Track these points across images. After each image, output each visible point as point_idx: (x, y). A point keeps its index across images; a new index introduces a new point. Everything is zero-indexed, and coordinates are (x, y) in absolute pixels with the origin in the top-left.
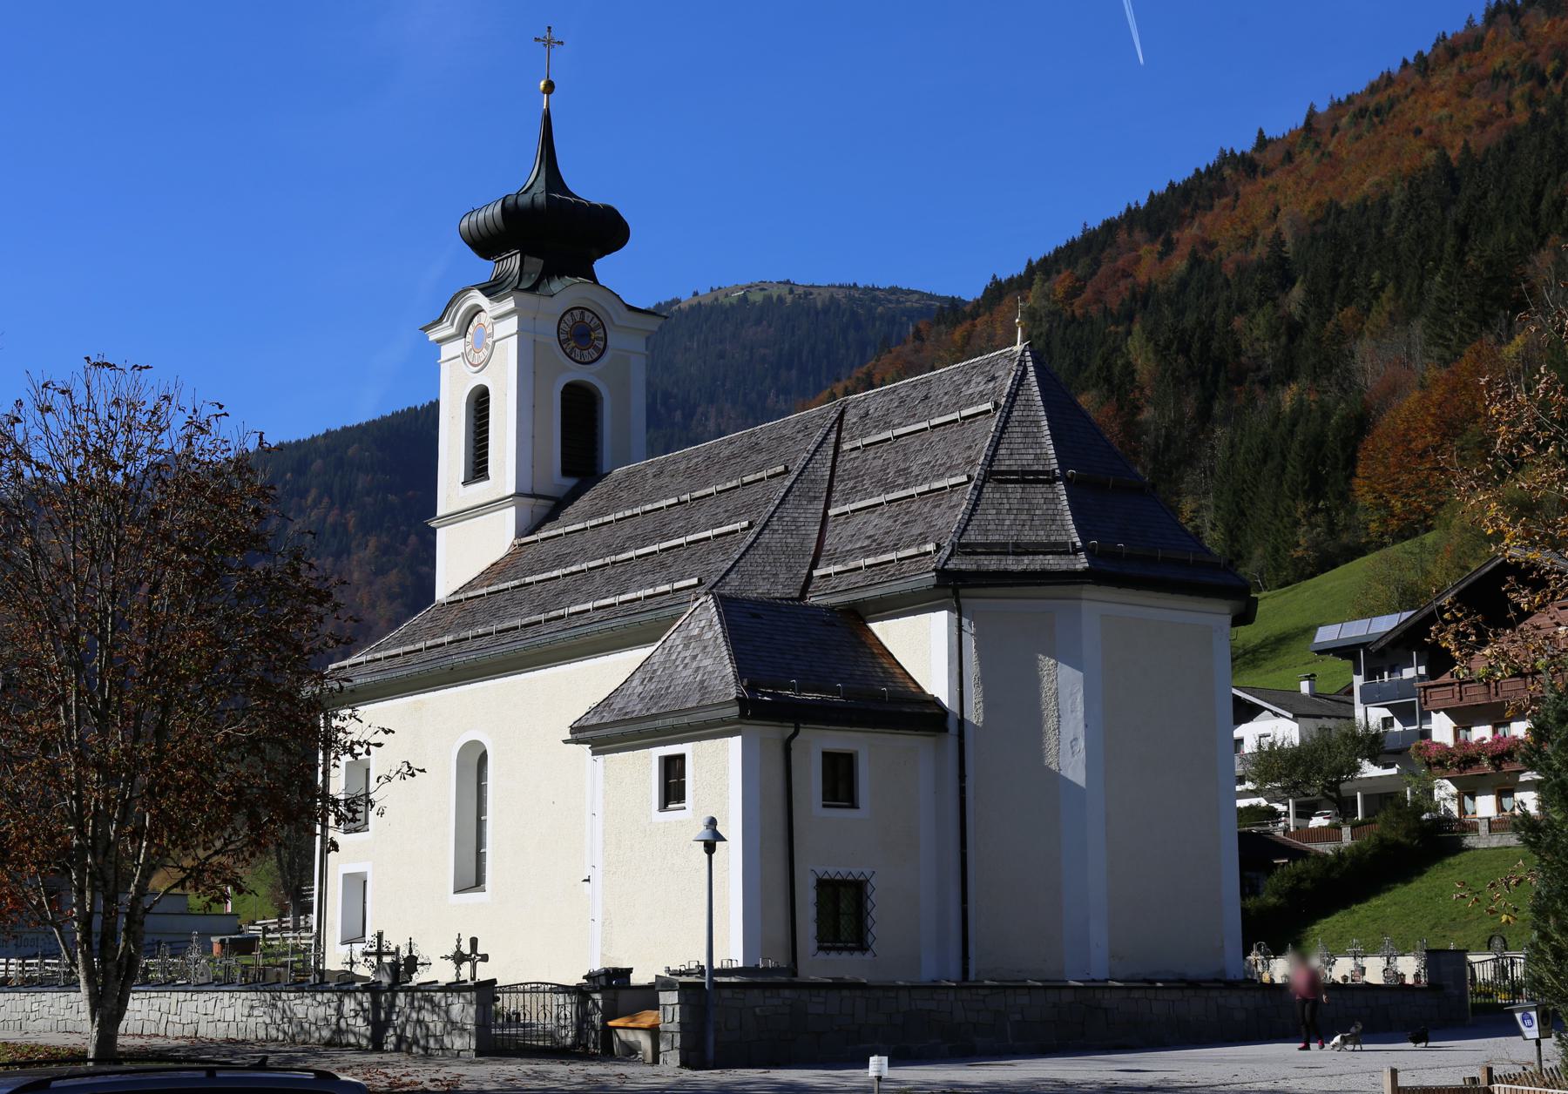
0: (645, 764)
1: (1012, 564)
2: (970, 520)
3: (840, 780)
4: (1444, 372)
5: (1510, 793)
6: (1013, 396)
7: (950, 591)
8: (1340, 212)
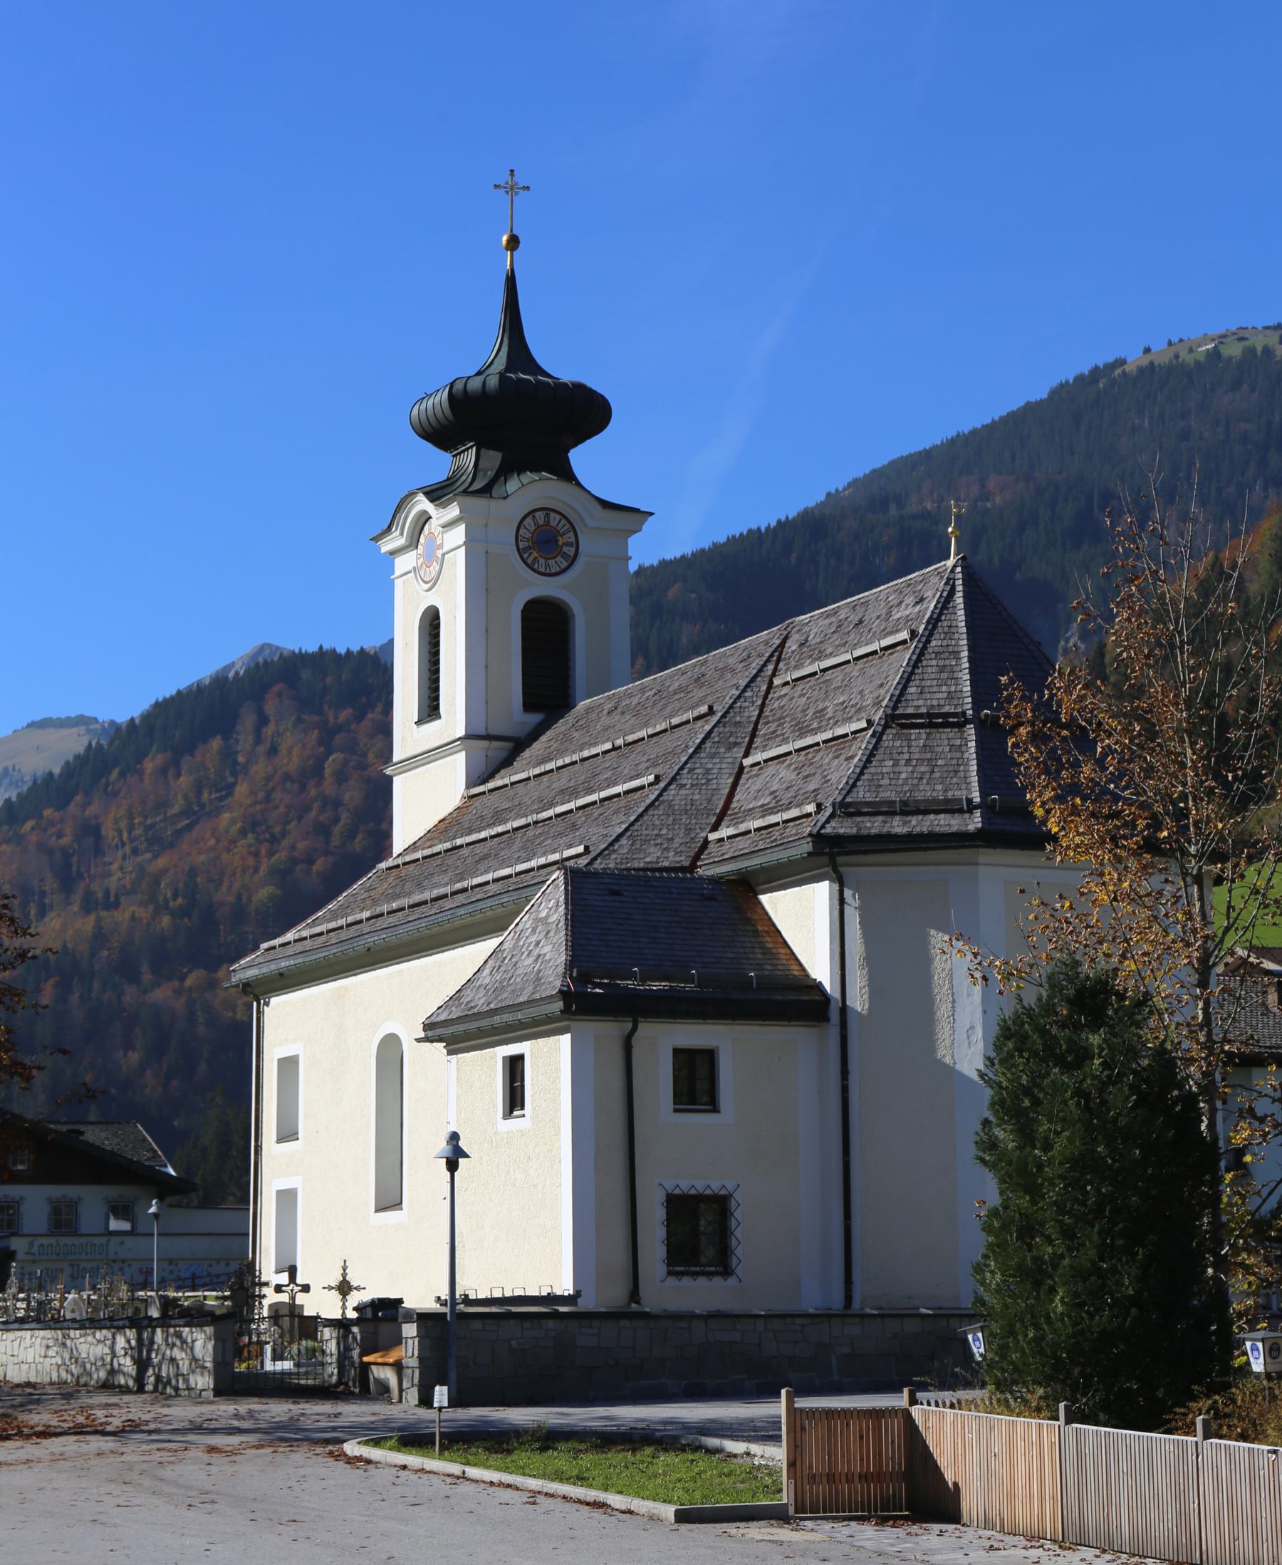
1: (898, 826)
2: (862, 773)
3: (696, 1082)
6: (934, 622)
7: (825, 859)
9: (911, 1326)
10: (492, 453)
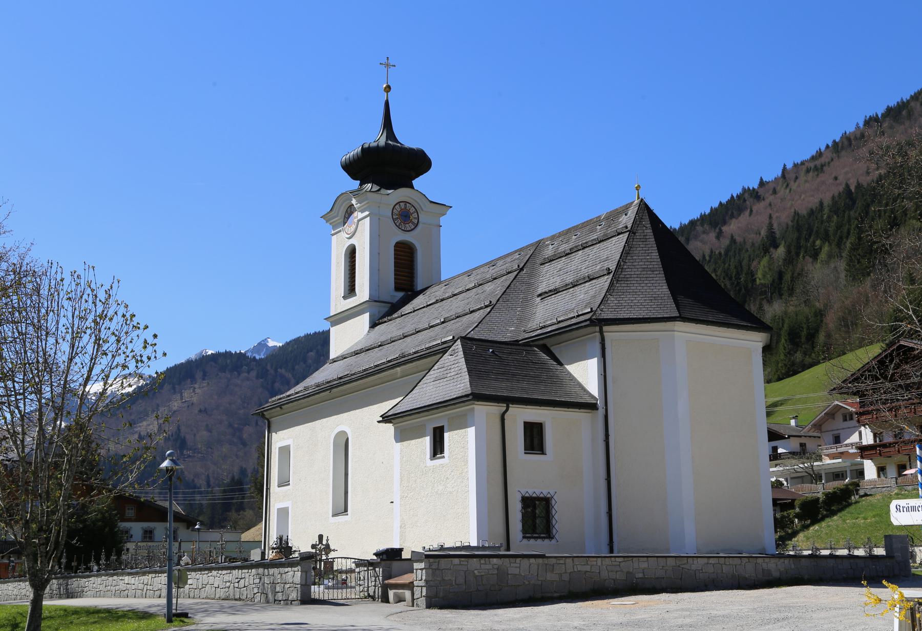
3: (534, 437)
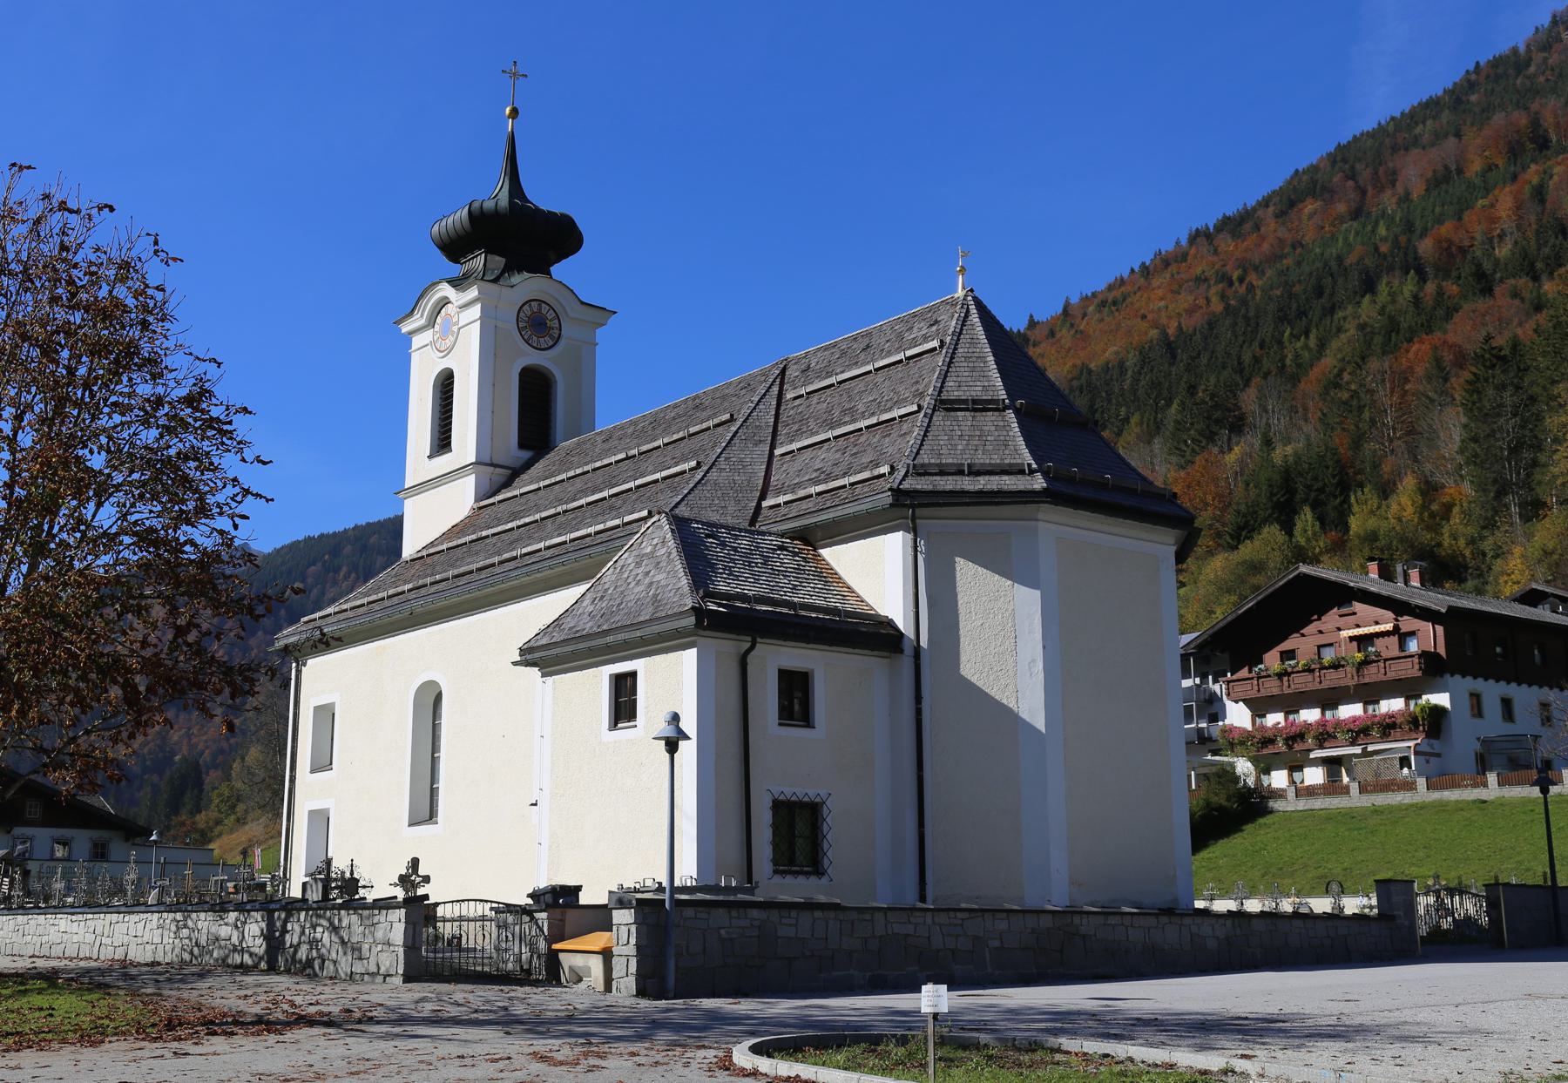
0: (596, 682)
3: (796, 697)
4: (1182, 474)
5: (1300, 768)
6: (958, 335)
8: (1090, 372)
9: (1046, 922)
10: (497, 258)
